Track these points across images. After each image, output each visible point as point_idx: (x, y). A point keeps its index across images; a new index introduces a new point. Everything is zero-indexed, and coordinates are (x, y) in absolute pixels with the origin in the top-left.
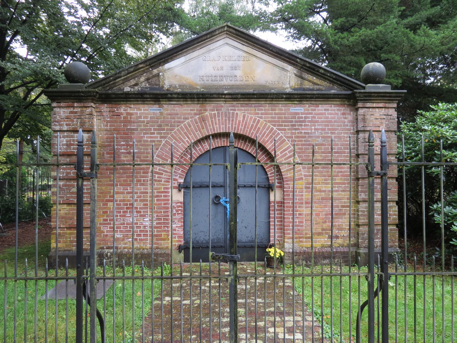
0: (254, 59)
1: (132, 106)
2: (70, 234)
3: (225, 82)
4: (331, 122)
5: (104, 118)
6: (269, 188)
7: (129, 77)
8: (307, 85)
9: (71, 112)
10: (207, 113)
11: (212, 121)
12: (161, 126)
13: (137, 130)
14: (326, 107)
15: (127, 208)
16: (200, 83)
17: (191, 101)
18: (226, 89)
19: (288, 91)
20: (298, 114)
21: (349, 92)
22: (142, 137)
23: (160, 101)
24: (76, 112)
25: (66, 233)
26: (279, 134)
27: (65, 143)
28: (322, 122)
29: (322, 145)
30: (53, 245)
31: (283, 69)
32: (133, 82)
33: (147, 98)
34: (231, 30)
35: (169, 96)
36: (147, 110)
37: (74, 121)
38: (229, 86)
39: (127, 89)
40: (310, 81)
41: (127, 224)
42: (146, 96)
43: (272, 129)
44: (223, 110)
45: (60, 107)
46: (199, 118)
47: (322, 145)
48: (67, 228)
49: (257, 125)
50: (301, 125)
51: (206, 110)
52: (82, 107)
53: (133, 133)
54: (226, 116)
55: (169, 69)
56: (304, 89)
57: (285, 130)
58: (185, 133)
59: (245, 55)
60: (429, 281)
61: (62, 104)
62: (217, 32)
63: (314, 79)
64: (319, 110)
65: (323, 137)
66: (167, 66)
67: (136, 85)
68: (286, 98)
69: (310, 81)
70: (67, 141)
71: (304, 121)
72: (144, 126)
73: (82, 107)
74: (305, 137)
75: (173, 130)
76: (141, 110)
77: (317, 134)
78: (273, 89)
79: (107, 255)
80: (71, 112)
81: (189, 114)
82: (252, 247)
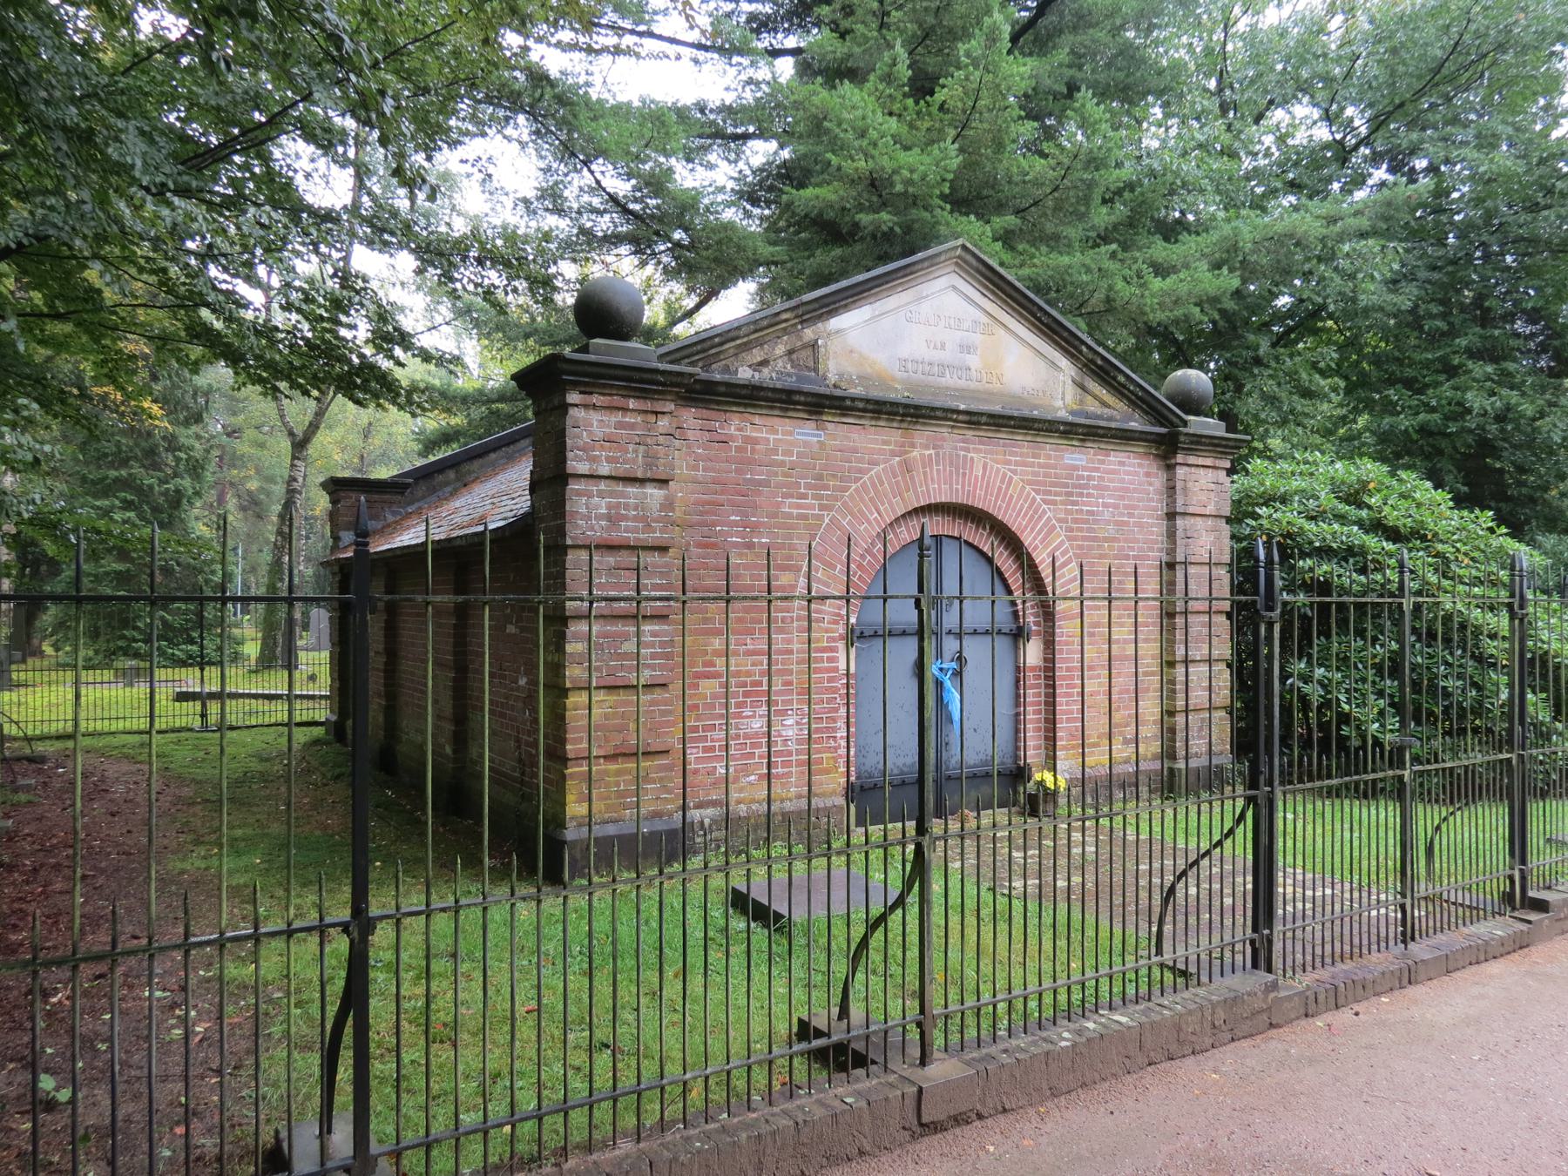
0: (1002, 332)
1: (757, 420)
2: (619, 773)
3: (949, 380)
4: (1127, 490)
5: (689, 447)
6: (1018, 635)
7: (750, 342)
8: (1092, 406)
9: (619, 425)
10: (915, 453)
11: (925, 473)
12: (820, 477)
13: (766, 483)
14: (1121, 457)
15: (746, 694)
16: (900, 375)
17: (781, 409)
18: (962, 398)
19: (1062, 414)
20: (1076, 468)
21: (1163, 430)
22: (779, 505)
23: (821, 413)
24: (632, 426)
25: (606, 772)
26: (1044, 512)
27: (604, 511)
28: (1115, 489)
29: (1114, 540)
30: (575, 808)
31: (1053, 364)
32: (757, 355)
33: (798, 403)
34: (969, 257)
35: (848, 403)
36: (791, 434)
37: (627, 452)
38: (956, 390)
39: (745, 374)
40: (1095, 397)
41: (746, 736)
42: (797, 398)
43: (1034, 500)
44: (947, 447)
45: (586, 406)
46: (900, 463)
47: (1114, 540)
48: (605, 757)
49: (1007, 488)
50: (1081, 495)
51: (913, 446)
52: (646, 412)
53: (759, 493)
54: (951, 464)
55: (838, 332)
56: (1087, 416)
57: (1054, 503)
58: (871, 499)
59: (985, 319)
60: (1319, 804)
61: (596, 399)
62: (943, 258)
63: (1103, 393)
64: (1110, 463)
65: (1117, 523)
66: (835, 323)
67: (764, 363)
68: (1064, 432)
69: (1095, 397)
70: (609, 507)
71: (1086, 486)
72: (785, 475)
73: (646, 412)
74: (1087, 522)
75: (846, 489)
76: (776, 432)
77: (1107, 516)
78: (1036, 407)
79: (702, 823)
80: (619, 425)
81: (881, 452)
82: (988, 775)
